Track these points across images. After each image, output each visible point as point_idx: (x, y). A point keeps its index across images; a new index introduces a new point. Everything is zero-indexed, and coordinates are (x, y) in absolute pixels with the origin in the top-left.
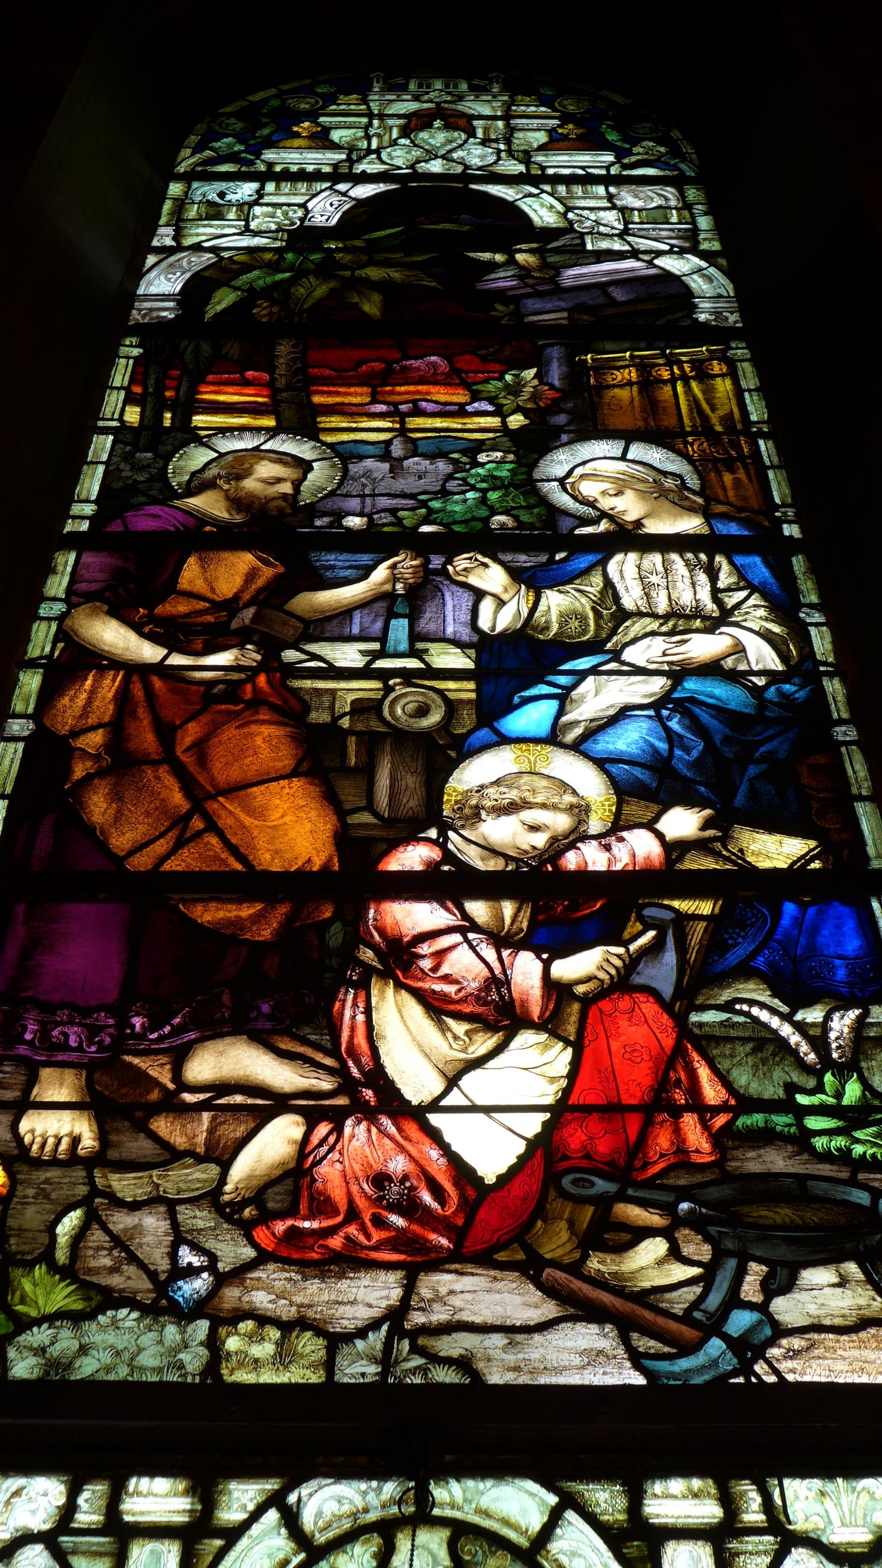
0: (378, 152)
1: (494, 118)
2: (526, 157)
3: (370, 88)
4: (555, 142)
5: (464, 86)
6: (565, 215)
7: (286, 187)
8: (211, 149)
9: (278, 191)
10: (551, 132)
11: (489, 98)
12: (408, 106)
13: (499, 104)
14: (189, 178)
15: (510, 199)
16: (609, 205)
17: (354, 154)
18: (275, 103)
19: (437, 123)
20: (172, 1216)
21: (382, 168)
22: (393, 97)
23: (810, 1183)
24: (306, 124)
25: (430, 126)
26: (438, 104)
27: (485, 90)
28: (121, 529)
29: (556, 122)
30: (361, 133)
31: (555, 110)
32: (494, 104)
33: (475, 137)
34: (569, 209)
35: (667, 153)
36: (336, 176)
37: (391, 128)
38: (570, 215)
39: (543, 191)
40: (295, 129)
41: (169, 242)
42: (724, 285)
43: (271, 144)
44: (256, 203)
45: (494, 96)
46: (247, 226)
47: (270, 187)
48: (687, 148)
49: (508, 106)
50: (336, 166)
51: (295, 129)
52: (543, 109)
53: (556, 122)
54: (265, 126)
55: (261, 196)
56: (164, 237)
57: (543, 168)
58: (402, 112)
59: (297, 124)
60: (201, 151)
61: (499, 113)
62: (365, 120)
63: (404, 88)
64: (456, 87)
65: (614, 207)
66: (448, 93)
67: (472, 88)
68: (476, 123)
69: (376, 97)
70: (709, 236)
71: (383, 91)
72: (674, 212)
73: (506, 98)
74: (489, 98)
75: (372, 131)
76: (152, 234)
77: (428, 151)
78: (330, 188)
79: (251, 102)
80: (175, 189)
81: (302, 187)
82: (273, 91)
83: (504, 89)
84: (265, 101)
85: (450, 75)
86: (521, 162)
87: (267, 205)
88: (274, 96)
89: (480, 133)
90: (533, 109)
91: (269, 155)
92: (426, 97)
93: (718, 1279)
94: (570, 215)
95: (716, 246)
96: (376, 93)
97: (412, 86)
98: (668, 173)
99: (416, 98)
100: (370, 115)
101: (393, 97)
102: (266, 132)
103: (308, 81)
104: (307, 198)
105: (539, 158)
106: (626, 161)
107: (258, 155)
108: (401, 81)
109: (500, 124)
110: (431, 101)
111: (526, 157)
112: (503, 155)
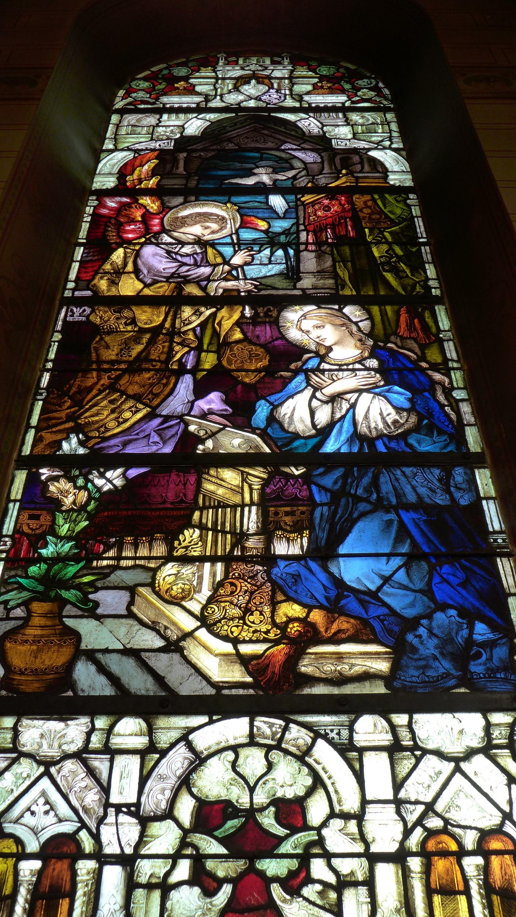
0: (221, 96)
1: (284, 78)
2: (300, 99)
3: (217, 63)
4: (316, 89)
5: (268, 61)
6: (322, 129)
7: (173, 116)
8: (131, 97)
9: (169, 119)
10: (315, 85)
11: (281, 68)
12: (237, 73)
13: (286, 71)
14: (123, 112)
15: (293, 121)
16: (345, 123)
17: (207, 98)
18: (165, 72)
19: (253, 82)
20: (310, 792)
21: (224, 105)
22: (231, 68)
23: (67, 900)
24: (182, 83)
25: (249, 83)
26: (254, 71)
27: (279, 63)
28: (371, 293)
29: (316, 80)
30: (212, 87)
31: (316, 73)
32: (283, 71)
33: (272, 88)
34: (323, 126)
35: (376, 95)
36: (199, 110)
37: (228, 84)
38: (325, 129)
39: (310, 117)
40: (176, 85)
41: (111, 147)
42: (405, 166)
43: (165, 93)
44: (158, 125)
45: (284, 67)
46: (152, 137)
47: (165, 117)
48: (386, 91)
49: (292, 72)
50: (198, 104)
51: (176, 85)
52: (311, 73)
53: (316, 80)
54: (160, 84)
55: (160, 122)
56: (109, 145)
57: (310, 104)
58: (233, 76)
59: (177, 83)
60: (126, 98)
61: (286, 76)
62: (213, 80)
63: (236, 63)
64: (264, 62)
65: (348, 124)
66: (261, 66)
67: (273, 62)
68: (273, 81)
69: (221, 68)
70: (397, 140)
71: (225, 64)
72: (380, 126)
73: (291, 68)
74: (281, 68)
75: (217, 86)
76: (103, 144)
77: (248, 96)
78: (196, 117)
79: (153, 72)
80: (115, 118)
81: (182, 116)
82: (164, 65)
83: (291, 62)
84: (161, 70)
85: (261, 53)
86: (297, 101)
87: (163, 126)
88: (165, 68)
89: (276, 86)
90: (305, 73)
91: (165, 99)
92: (247, 68)
93: (462, 881)
94: (325, 129)
95: (401, 146)
96: (221, 66)
97: (241, 61)
98: (373, 105)
99: (242, 69)
100: (217, 78)
101: (231, 68)
102: (162, 87)
103: (184, 60)
104: (184, 122)
105: (306, 98)
106: (354, 99)
107: (157, 99)
108: (234, 59)
109: (287, 81)
110: (250, 70)
111: (300, 98)
112: (287, 97)
